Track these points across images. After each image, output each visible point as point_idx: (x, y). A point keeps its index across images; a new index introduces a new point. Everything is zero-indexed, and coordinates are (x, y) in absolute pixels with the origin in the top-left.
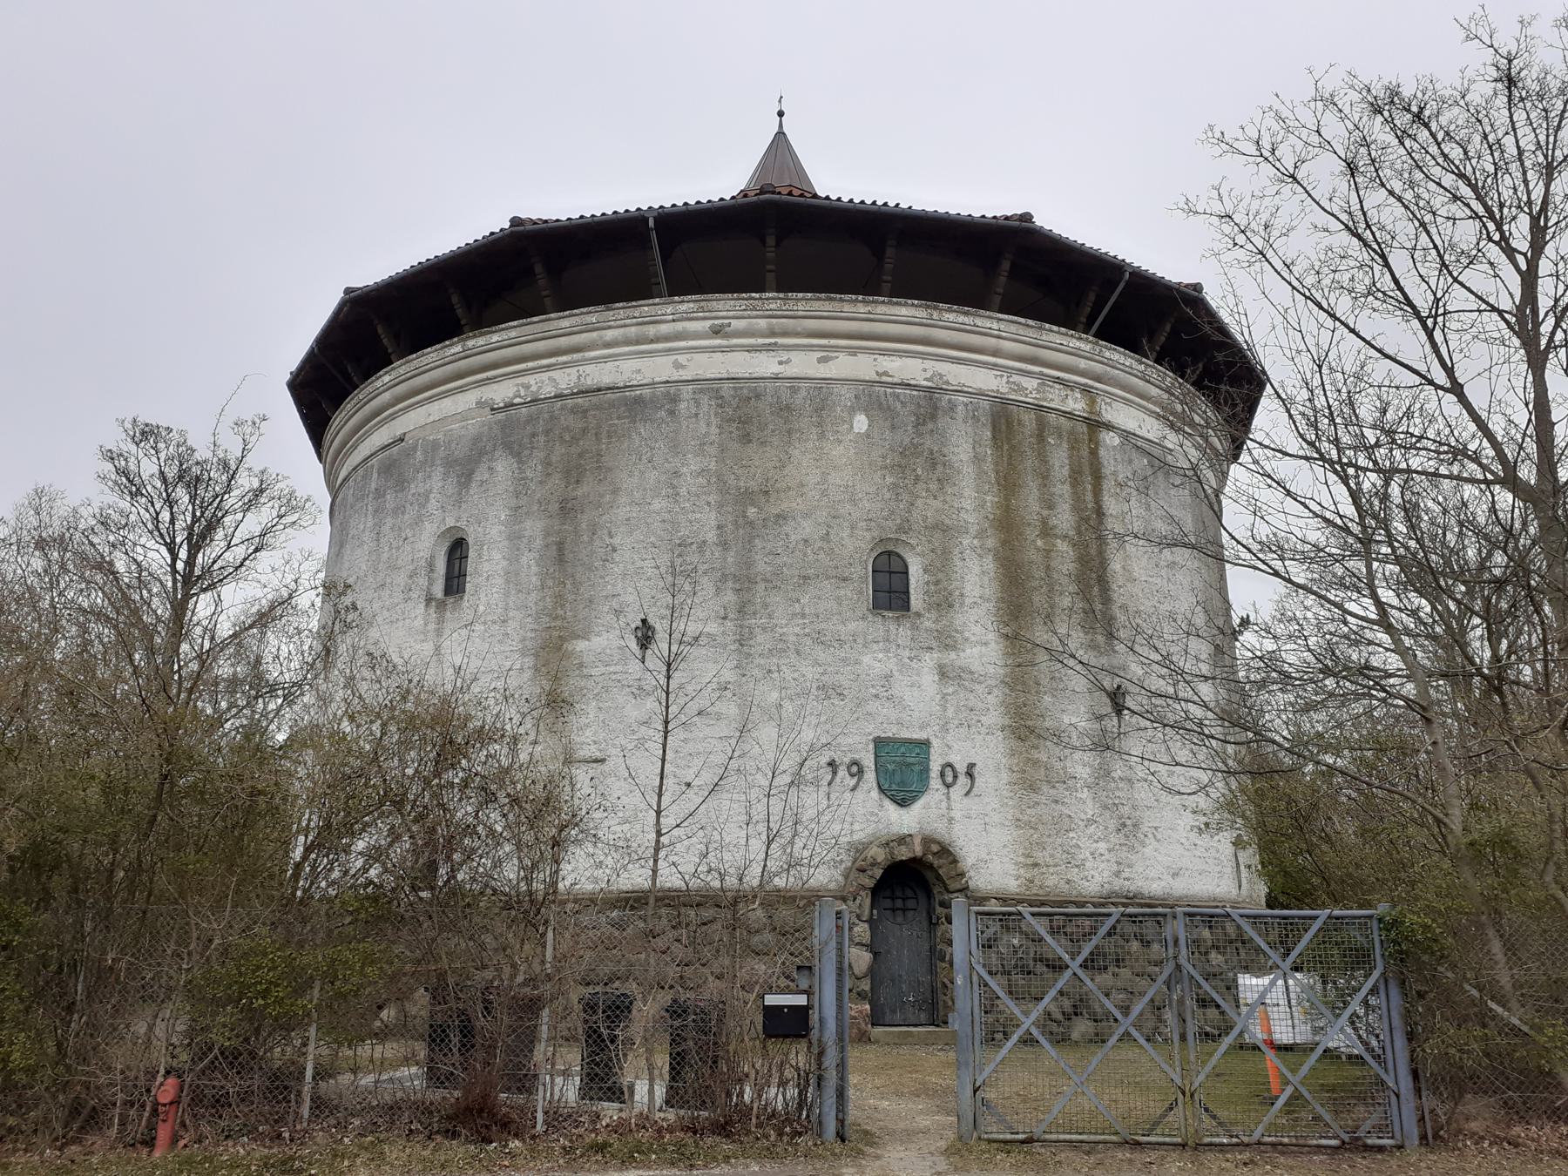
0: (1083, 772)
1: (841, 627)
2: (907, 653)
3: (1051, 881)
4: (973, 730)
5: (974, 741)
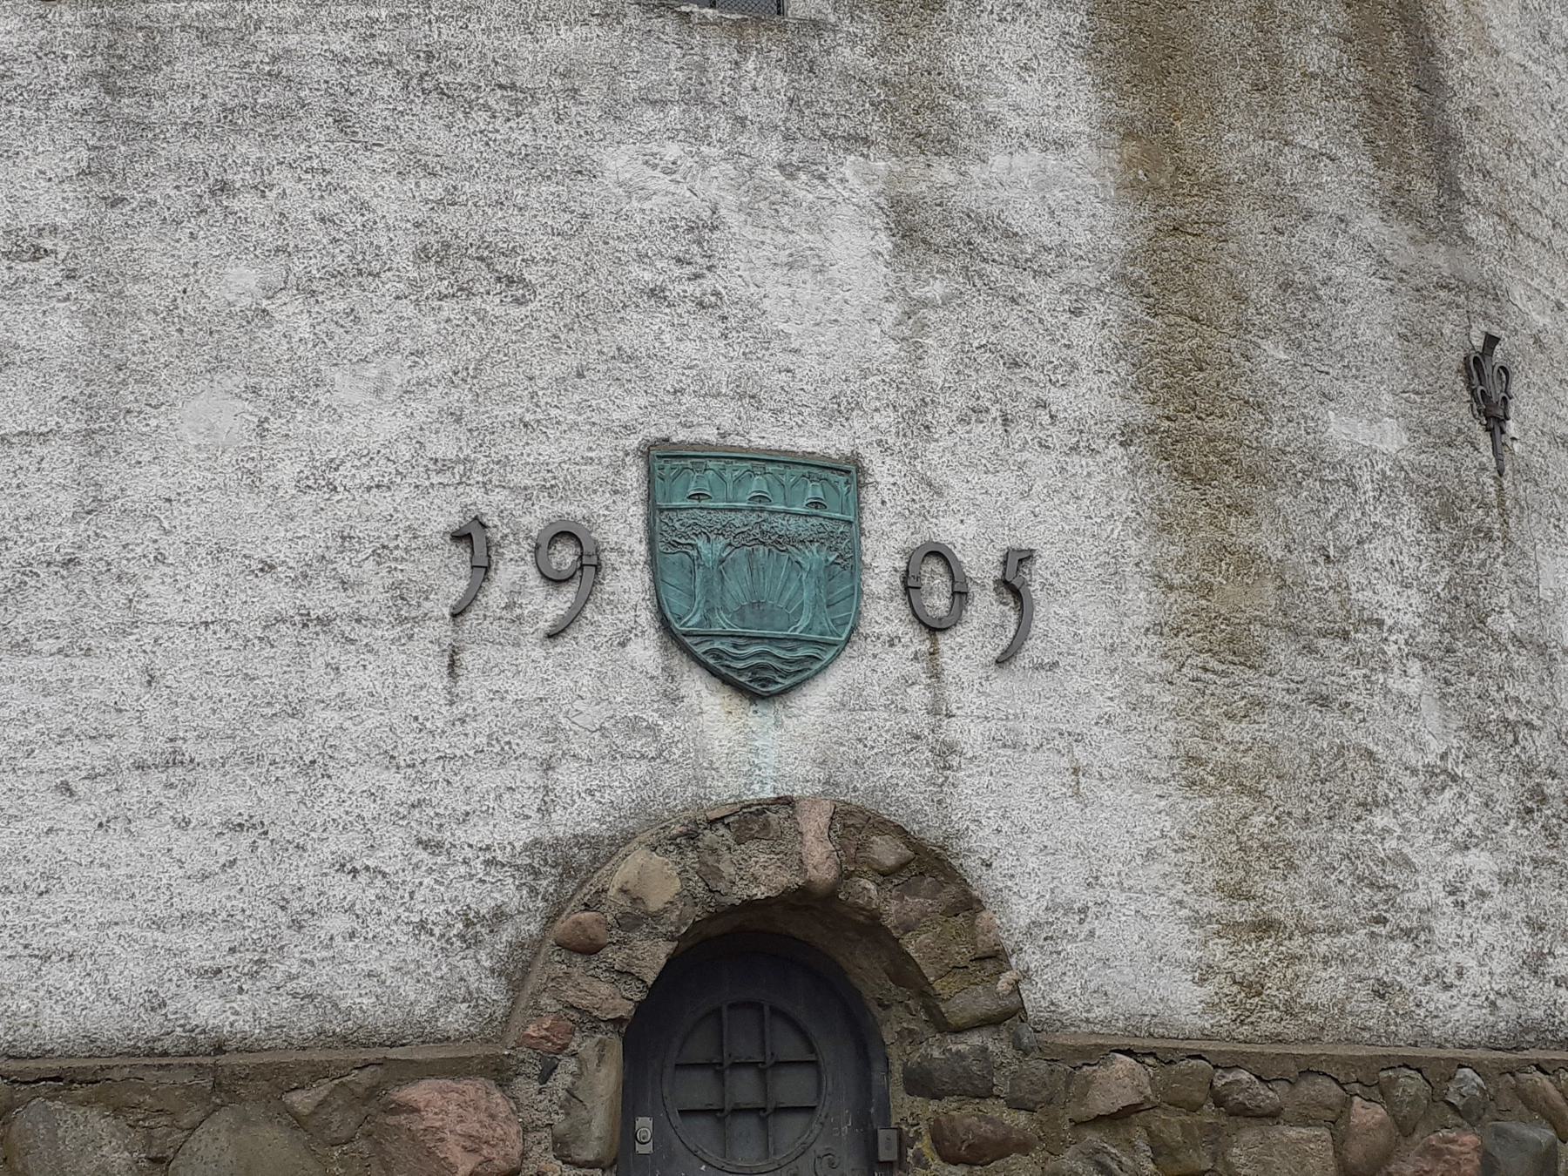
0: (1402, 608)
1: (515, 40)
2: (773, 149)
3: (1325, 986)
4: (1021, 432)
5: (1025, 473)
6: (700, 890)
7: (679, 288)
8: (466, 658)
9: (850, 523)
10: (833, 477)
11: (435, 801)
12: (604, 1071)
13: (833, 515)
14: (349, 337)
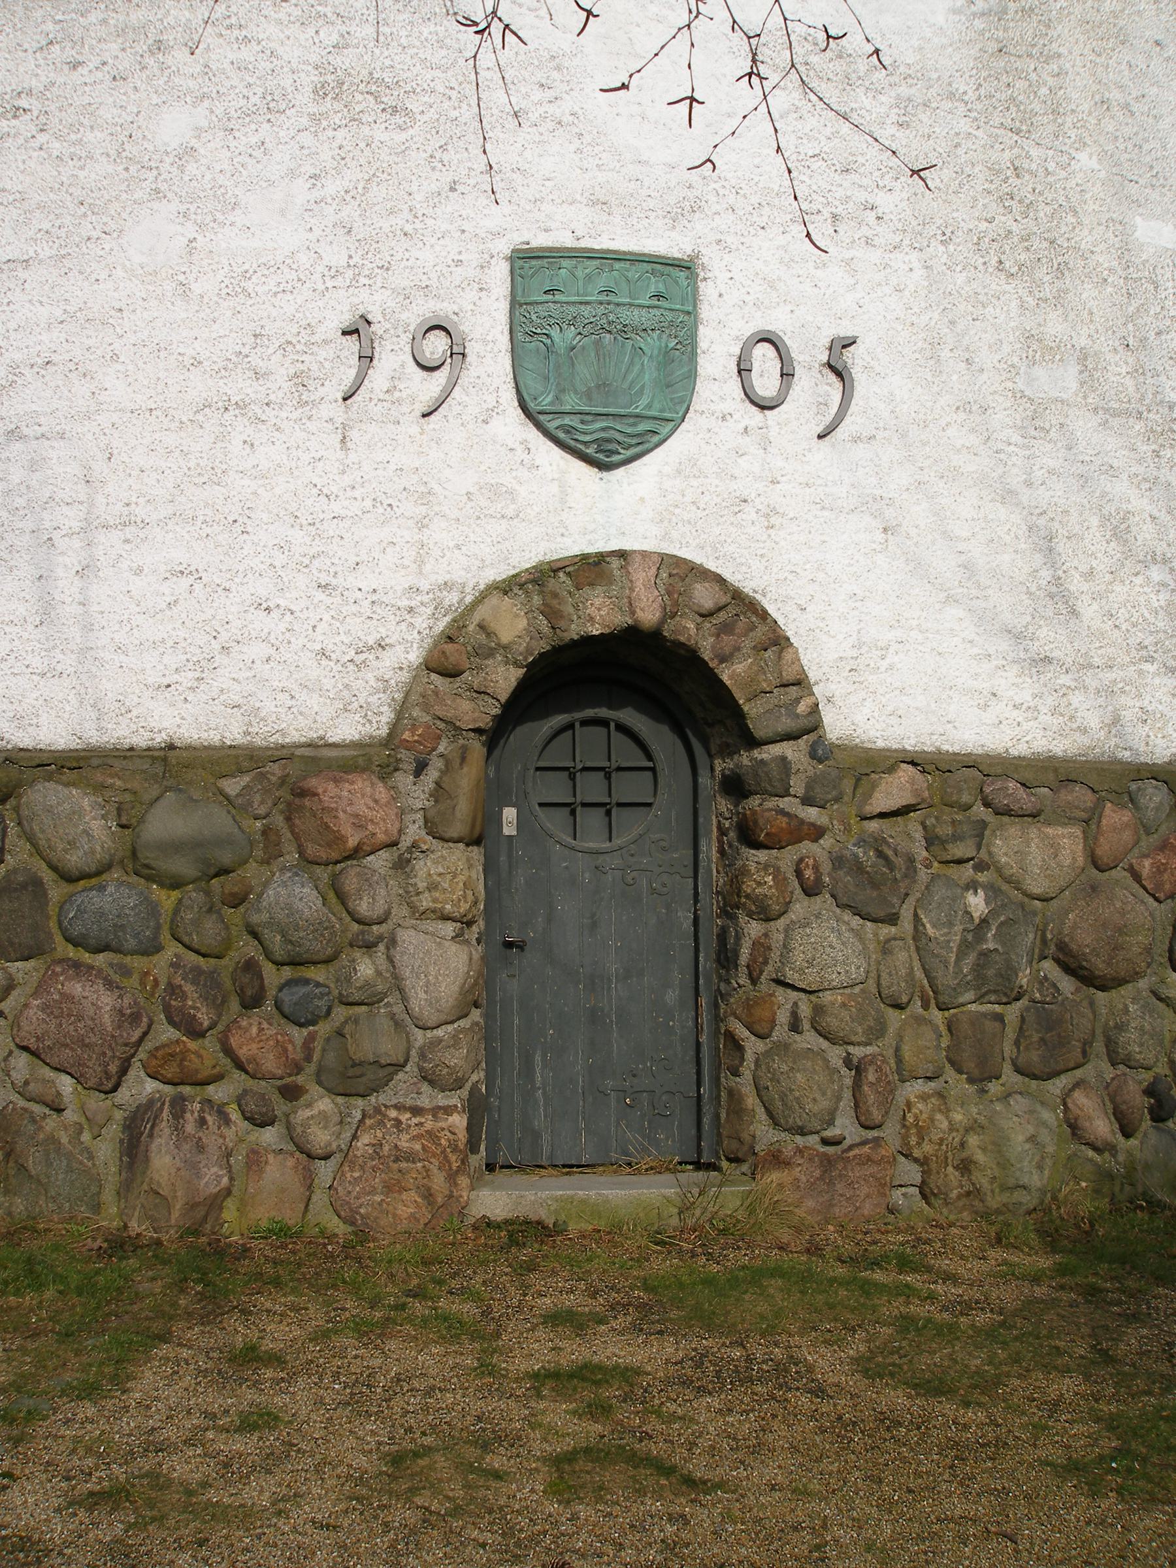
6: (546, 630)
7: (541, 110)
8: (354, 434)
9: (689, 313)
10: (676, 272)
11: (331, 553)
12: (465, 769)
13: (673, 307)
14: (260, 166)
